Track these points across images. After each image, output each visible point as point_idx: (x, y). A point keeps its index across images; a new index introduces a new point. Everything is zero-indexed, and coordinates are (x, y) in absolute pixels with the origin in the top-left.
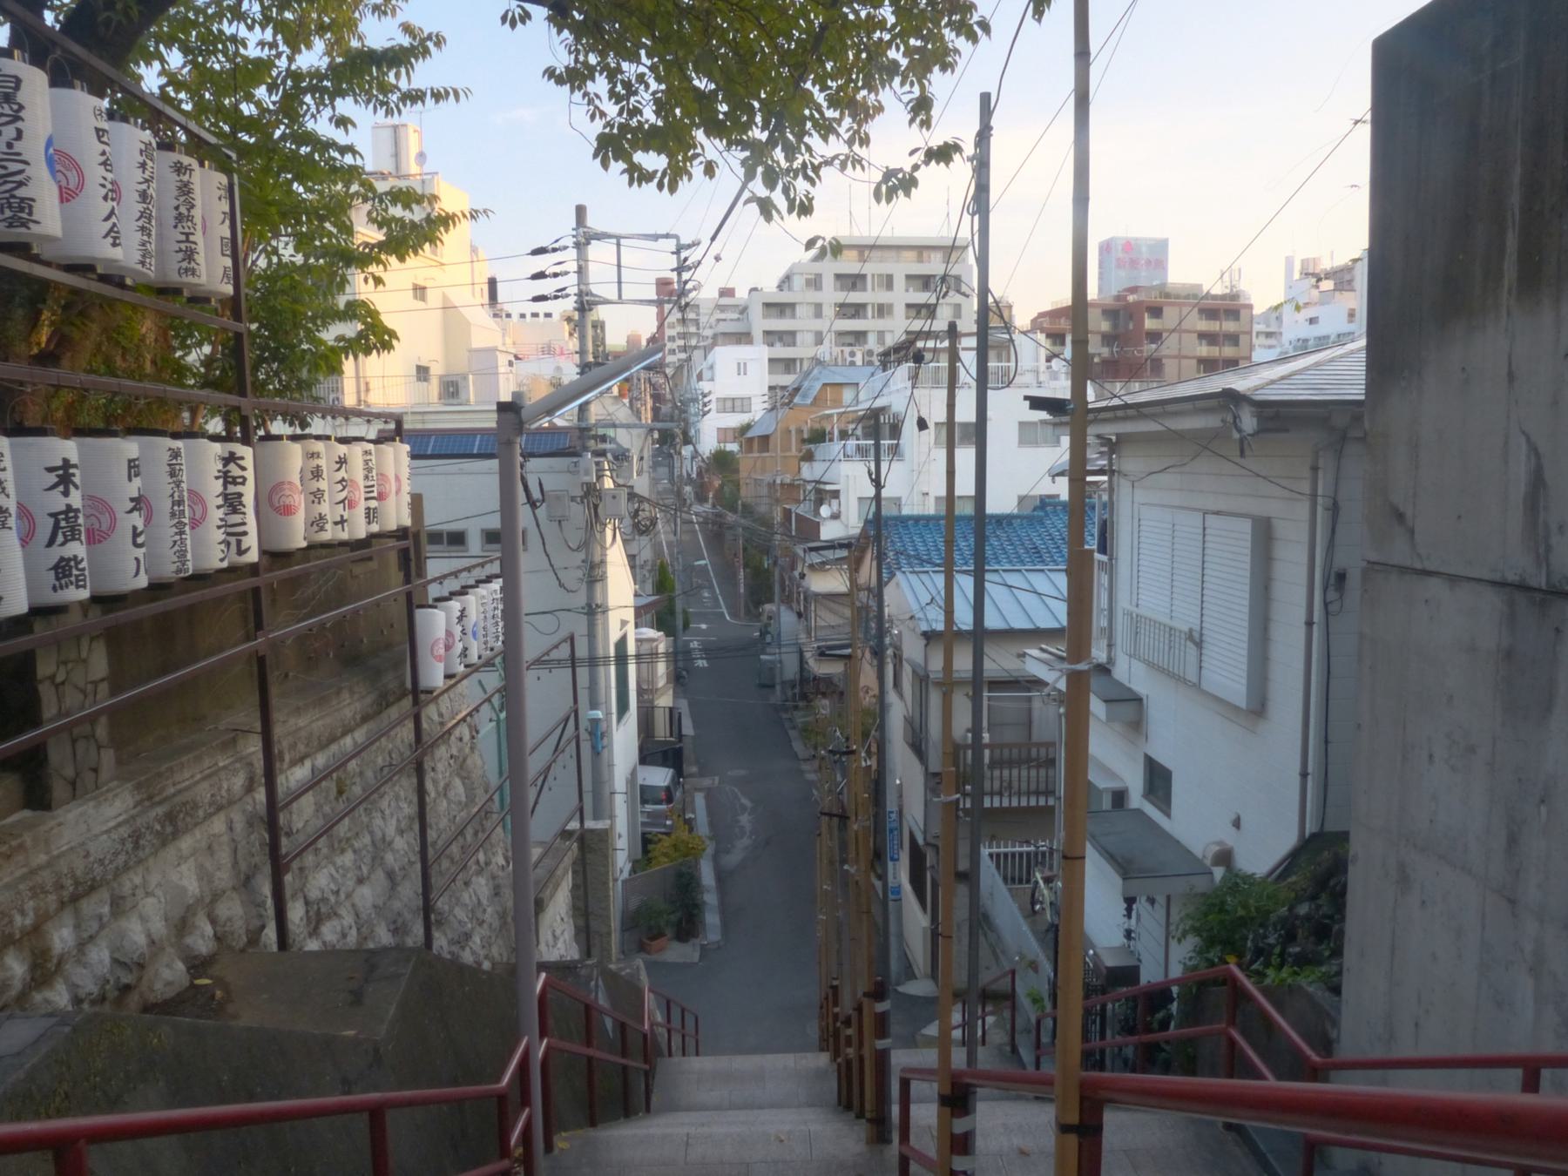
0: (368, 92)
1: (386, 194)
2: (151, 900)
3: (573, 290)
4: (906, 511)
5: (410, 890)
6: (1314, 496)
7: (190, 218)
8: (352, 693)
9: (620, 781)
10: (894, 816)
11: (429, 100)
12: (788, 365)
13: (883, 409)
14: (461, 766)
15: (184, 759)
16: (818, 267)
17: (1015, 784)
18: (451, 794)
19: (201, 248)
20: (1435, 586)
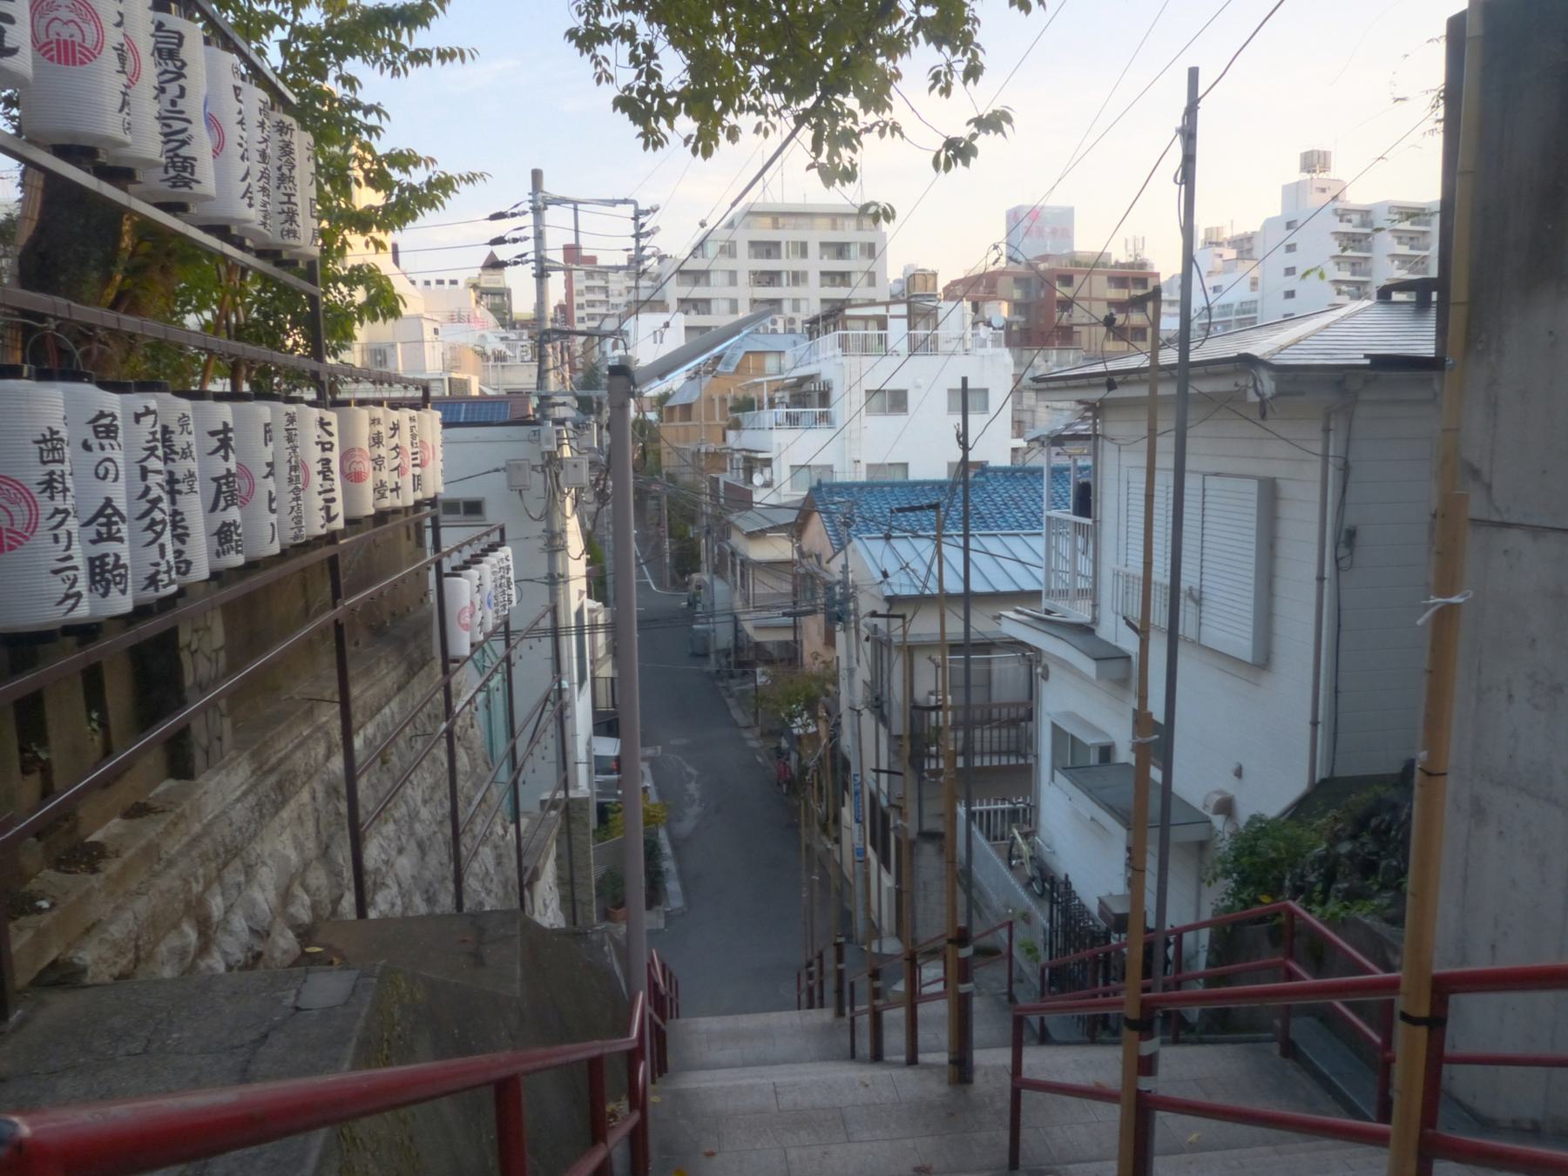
0: (378, 56)
1: (386, 156)
2: (265, 869)
3: (532, 256)
4: (839, 478)
5: (439, 856)
6: (1325, 456)
7: (291, 179)
8: (388, 663)
11: (435, 62)
13: (810, 378)
15: (281, 728)
20: (1514, 538)
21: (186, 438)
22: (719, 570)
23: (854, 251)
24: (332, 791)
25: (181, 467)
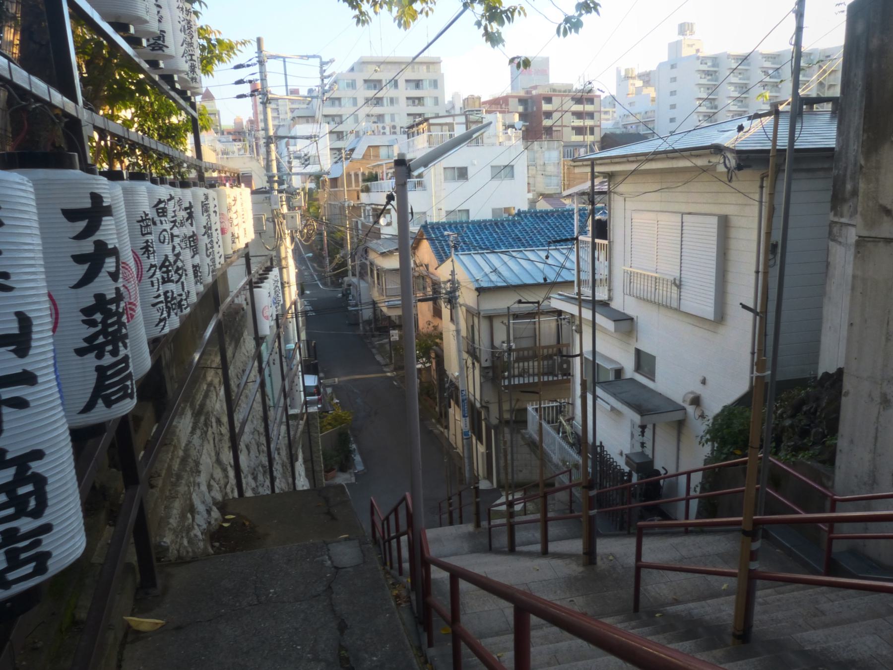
4: (472, 218)
6: (761, 202)
16: (353, 76)
17: (531, 371)
22: (362, 276)
23: (426, 84)
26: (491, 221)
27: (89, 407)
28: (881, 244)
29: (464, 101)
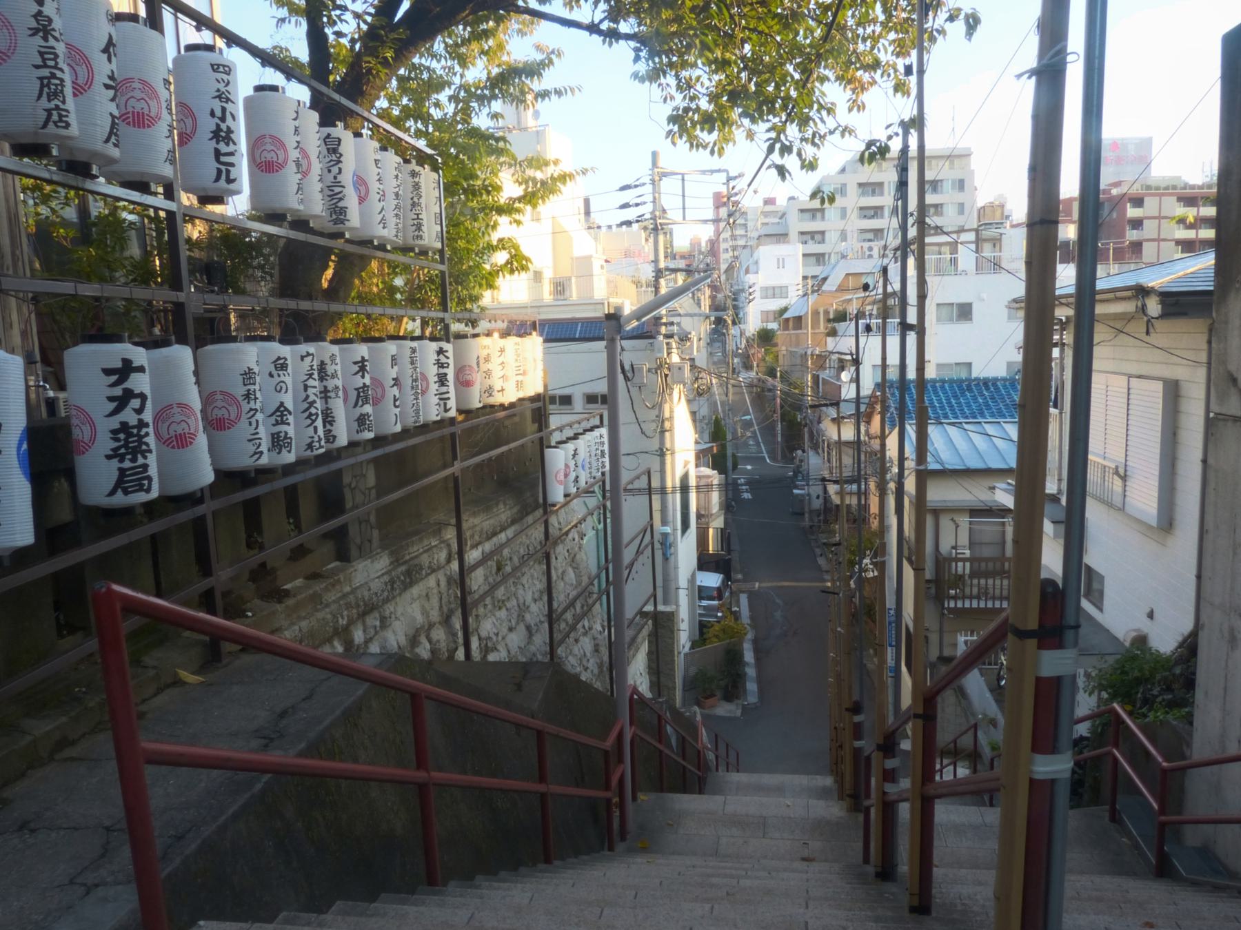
4: (975, 374)
8: (505, 504)
9: (683, 581)
10: (892, 612)
11: (554, 97)
12: (820, 258)
14: (573, 561)
17: (991, 591)
18: (566, 578)
19: (425, 223)
21: (334, 367)
23: (947, 186)
24: (450, 580)
25: (331, 384)
26: (1004, 379)
27: (112, 493)
28: (1230, 424)
29: (979, 211)
